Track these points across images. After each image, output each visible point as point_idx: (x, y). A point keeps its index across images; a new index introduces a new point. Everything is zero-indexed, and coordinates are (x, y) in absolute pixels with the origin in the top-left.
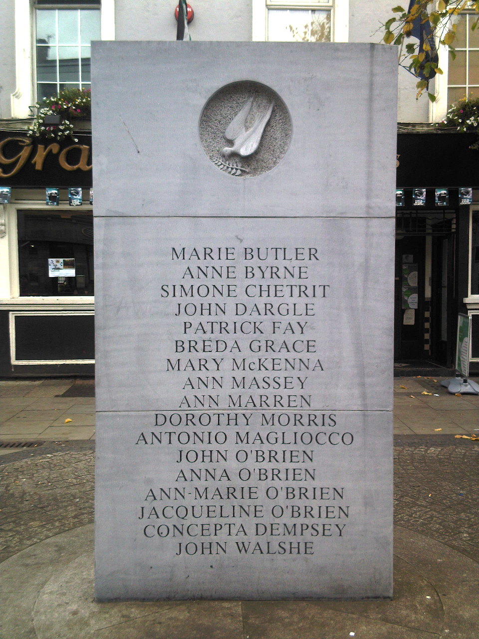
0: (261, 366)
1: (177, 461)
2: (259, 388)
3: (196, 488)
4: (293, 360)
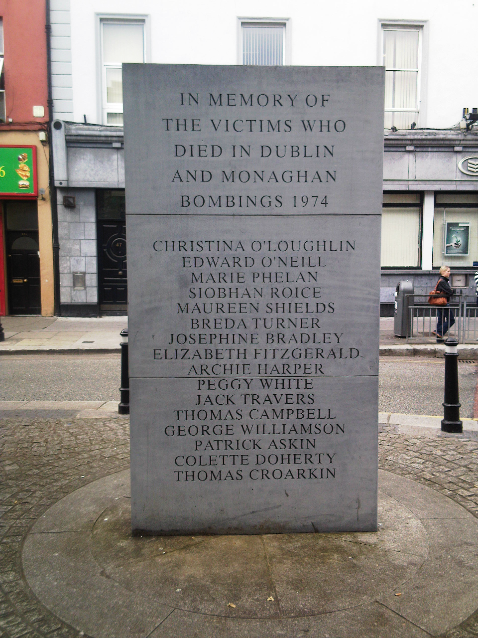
0: (292, 445)
1: (196, 404)
2: (276, 448)
3: (210, 196)
4: (332, 147)
